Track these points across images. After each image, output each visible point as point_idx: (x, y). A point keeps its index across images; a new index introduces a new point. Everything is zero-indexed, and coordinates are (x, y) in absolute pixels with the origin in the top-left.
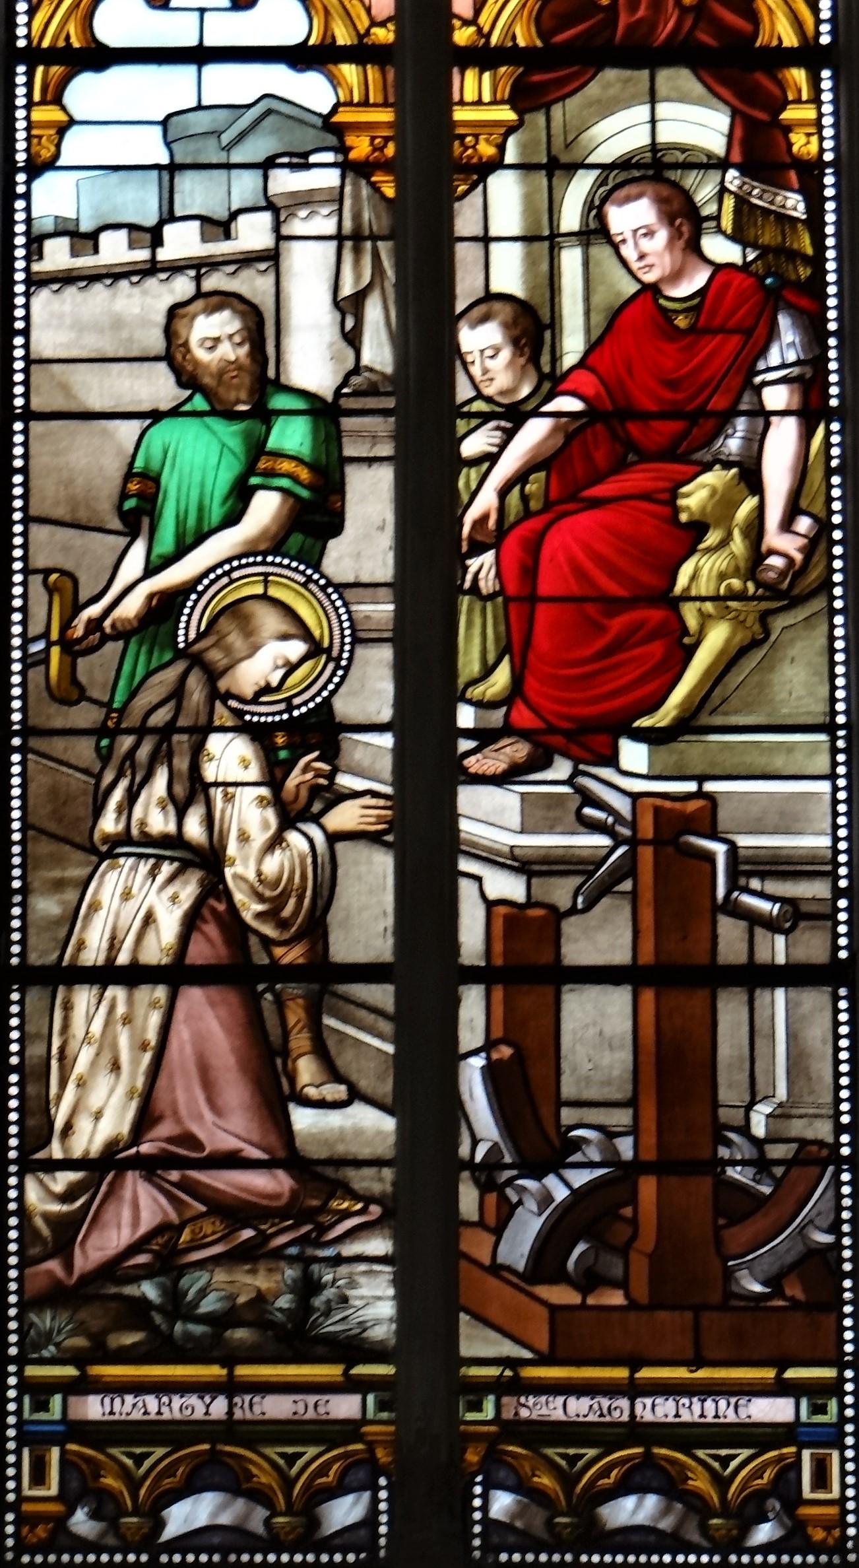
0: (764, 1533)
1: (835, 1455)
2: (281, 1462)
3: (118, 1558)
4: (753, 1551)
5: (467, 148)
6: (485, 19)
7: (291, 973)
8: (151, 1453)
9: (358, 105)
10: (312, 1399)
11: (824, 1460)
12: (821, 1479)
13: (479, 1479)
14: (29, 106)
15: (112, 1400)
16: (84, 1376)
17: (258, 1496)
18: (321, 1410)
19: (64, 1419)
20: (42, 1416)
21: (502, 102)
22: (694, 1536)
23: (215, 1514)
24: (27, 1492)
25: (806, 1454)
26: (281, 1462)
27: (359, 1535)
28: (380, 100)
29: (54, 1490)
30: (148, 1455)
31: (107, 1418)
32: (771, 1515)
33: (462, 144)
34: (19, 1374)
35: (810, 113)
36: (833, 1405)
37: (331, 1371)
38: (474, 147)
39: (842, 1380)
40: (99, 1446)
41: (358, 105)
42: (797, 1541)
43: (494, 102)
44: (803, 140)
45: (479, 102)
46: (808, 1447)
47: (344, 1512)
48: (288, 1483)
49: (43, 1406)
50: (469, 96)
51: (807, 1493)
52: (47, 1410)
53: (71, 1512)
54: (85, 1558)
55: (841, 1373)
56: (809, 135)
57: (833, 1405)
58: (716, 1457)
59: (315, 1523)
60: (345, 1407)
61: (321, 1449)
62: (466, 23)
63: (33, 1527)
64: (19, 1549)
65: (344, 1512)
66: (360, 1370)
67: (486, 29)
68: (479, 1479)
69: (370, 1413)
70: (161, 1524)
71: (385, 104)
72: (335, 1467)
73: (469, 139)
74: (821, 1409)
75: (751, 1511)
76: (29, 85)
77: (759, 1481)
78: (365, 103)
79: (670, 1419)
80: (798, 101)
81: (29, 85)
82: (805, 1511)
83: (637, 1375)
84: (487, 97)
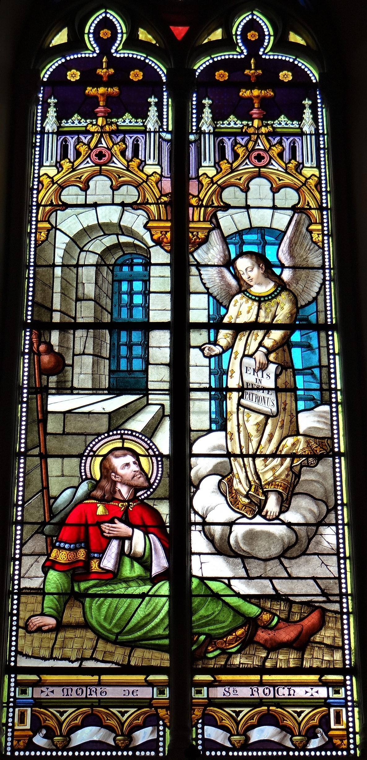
0: (314, 743)
1: (344, 710)
2: (234, 715)
3: (54, 754)
4: (310, 750)
5: (194, 236)
6: (201, 196)
7: (199, 524)
8: (243, 711)
9: (197, 222)
10: (131, 689)
11: (340, 712)
12: (338, 720)
13: (200, 721)
14: (37, 221)
15: (67, 690)
16: (215, 680)
17: (285, 729)
18: (135, 694)
19: (208, 698)
20: (200, 696)
21: (208, 221)
22: (289, 744)
23: (274, 736)
24: (16, 727)
25: (332, 710)
26: (234, 715)
27: (151, 745)
28: (165, 218)
29: (28, 727)
30: (66, 712)
31: (65, 697)
32: (319, 735)
33: (192, 234)
34: (15, 678)
35: (320, 227)
36: (342, 690)
37: (314, 678)
38: (165, 235)
39: (345, 680)
40: (107, 707)
41: (197, 222)
42: (330, 746)
43: (204, 221)
44: (317, 236)
45: (199, 221)
46: (17, 708)
47: (143, 735)
48: (122, 724)
49: (24, 692)
50: (196, 219)
51: (333, 726)
52: (26, 693)
53: (34, 735)
54: (25, 753)
55: (345, 678)
56: (318, 234)
57: (342, 690)
58: (234, 712)
59: (248, 738)
60: (146, 693)
61: (136, 709)
62: (194, 196)
63: (19, 741)
64: (13, 751)
65: (143, 735)
66: (151, 678)
67: (202, 198)
68: (200, 721)
69: (331, 696)
70: (70, 741)
71: (167, 220)
72: (142, 717)
73: (195, 233)
74: (337, 692)
75: (311, 734)
76: (37, 213)
77: (252, 721)
78: (160, 220)
79: (286, 696)
80: (316, 223)
81: (37, 213)
82: (331, 733)
83: (323, 678)
84: (202, 220)
